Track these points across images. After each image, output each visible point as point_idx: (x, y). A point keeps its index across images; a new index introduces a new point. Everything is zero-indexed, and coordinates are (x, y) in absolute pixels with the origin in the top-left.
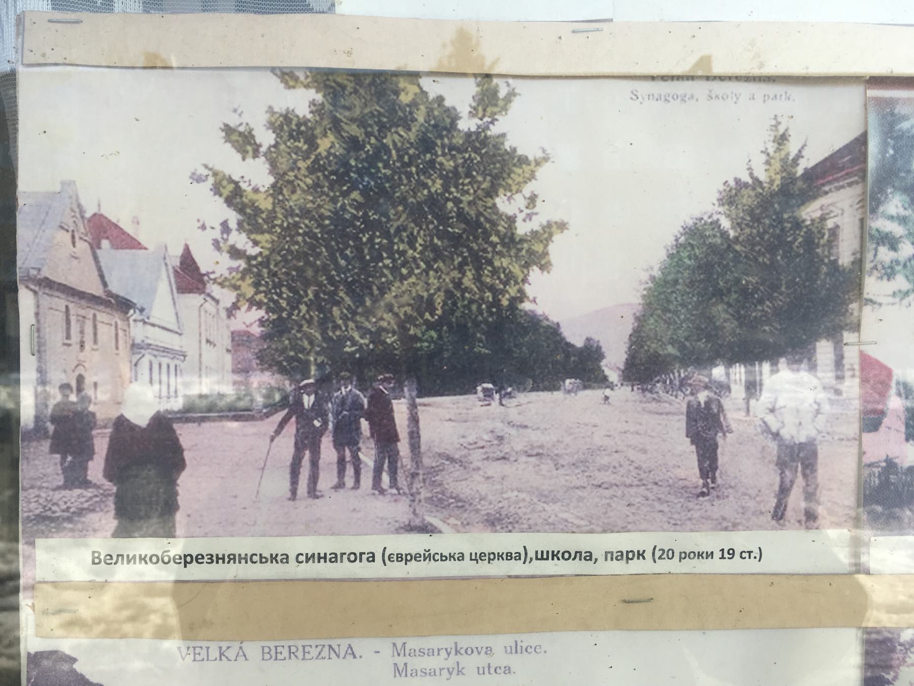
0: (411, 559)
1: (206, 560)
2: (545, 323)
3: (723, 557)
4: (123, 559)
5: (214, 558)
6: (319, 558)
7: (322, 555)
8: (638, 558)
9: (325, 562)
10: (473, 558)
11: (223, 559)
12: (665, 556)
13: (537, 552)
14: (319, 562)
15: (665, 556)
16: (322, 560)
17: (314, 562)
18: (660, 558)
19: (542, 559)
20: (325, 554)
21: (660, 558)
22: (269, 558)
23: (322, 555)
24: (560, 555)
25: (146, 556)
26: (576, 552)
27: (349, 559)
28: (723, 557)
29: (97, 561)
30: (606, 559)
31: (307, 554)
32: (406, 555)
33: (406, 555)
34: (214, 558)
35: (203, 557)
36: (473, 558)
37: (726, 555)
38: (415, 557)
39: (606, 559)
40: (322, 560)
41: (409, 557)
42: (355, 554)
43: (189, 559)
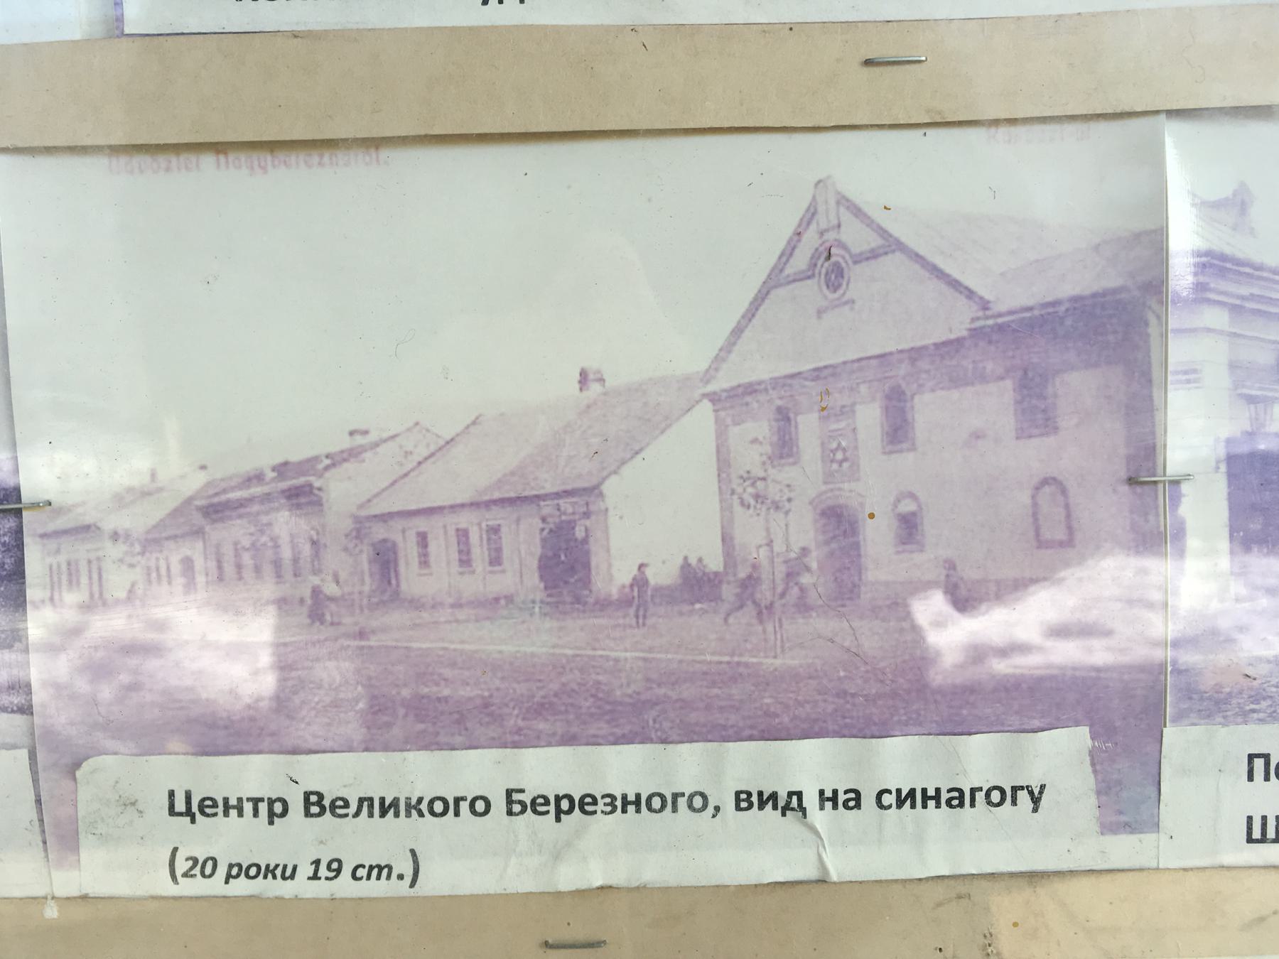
0: (238, 875)
1: (600, 807)
2: (264, 704)
3: (315, 877)
4: (371, 806)
5: (619, 803)
6: (637, 802)
7: (931, 793)
8: (265, 877)
9: (938, 806)
10: (180, 806)
11: (925, 797)
12: (197, 871)
13: (172, 794)
14: (925, 806)
15: (197, 871)
16: (931, 803)
17: (913, 806)
18: (185, 875)
19: (380, 868)
20: (938, 790)
21: (185, 875)
22: (198, 815)
23: (931, 793)
24: (424, 807)
25: (420, 800)
26: (361, 800)
27: (690, 806)
28: (315, 877)
29: (744, 805)
30: (1251, 777)
31: (899, 791)
32: (558, 799)
33: (558, 799)
34: (755, 799)
35: (595, 802)
36: (180, 806)
37: (323, 872)
38: (333, 806)
39: (1251, 777)
40: (931, 803)
41: (565, 805)
42: (662, 796)
43: (565, 805)
